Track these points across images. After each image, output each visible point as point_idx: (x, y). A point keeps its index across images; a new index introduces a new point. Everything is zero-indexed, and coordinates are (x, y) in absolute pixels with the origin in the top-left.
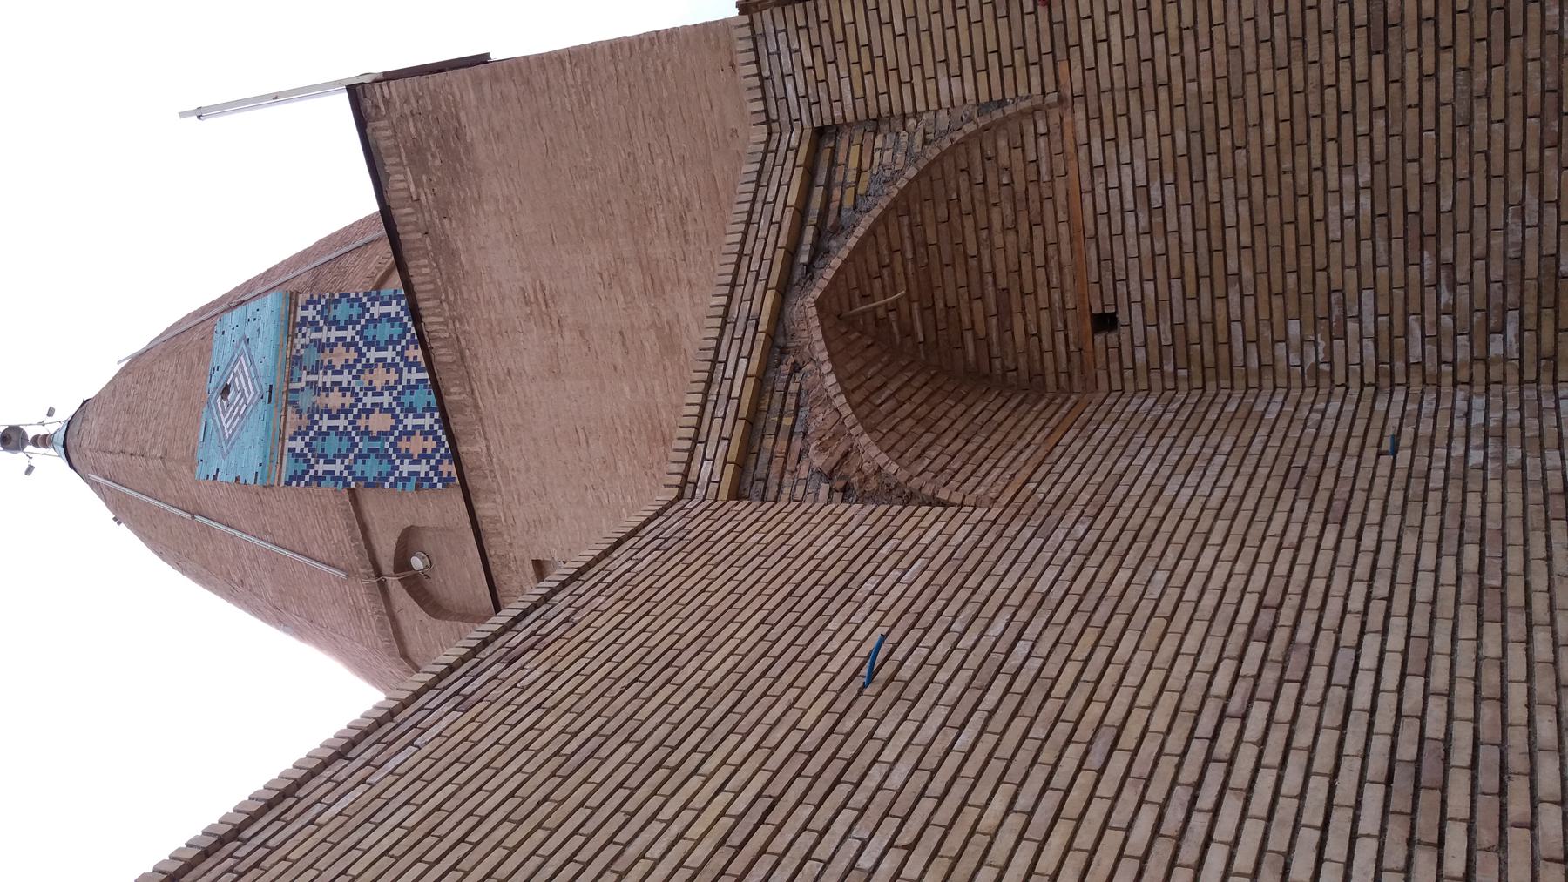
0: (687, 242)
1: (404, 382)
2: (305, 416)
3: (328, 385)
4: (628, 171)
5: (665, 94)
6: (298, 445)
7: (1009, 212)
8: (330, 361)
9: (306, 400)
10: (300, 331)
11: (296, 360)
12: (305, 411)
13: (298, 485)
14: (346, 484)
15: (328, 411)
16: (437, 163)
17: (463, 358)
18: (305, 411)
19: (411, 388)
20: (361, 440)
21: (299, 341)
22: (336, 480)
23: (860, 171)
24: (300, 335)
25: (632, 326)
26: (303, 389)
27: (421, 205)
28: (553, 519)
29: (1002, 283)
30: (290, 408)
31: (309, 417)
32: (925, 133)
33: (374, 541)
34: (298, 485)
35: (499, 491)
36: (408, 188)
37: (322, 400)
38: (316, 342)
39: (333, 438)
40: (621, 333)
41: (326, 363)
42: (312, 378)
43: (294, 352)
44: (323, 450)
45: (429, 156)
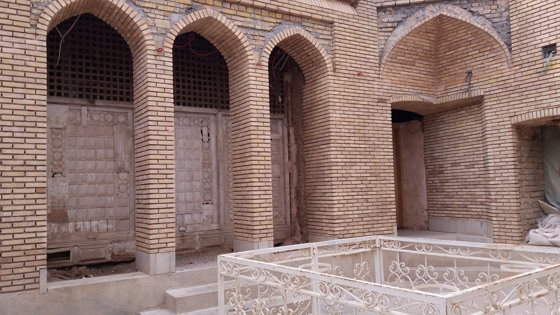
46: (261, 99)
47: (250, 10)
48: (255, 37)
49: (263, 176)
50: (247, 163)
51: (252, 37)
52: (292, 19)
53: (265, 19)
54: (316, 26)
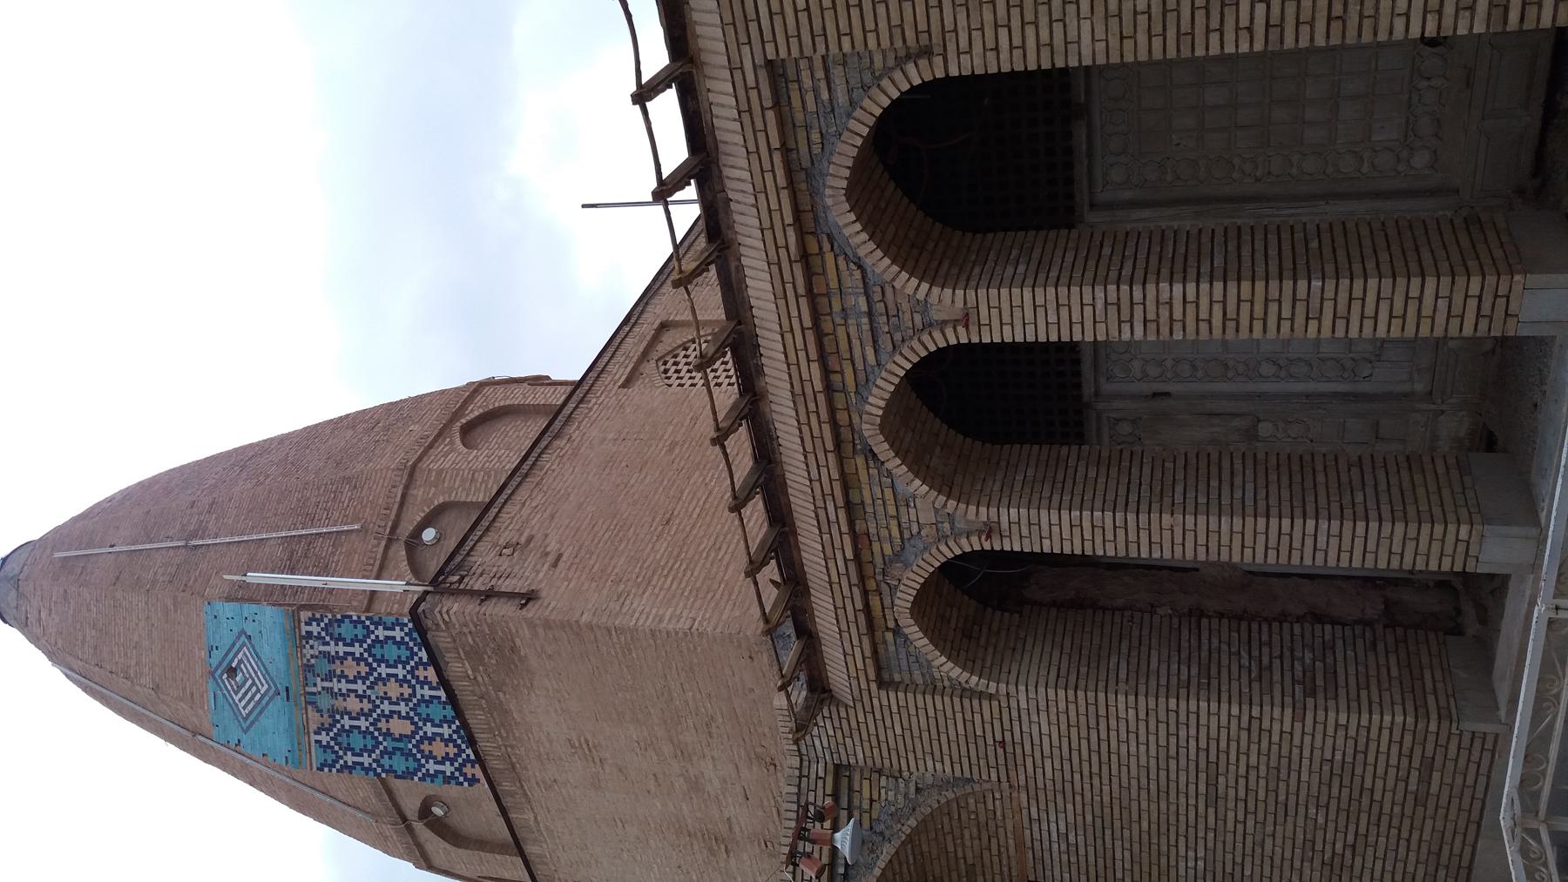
0: (711, 737)
1: (419, 697)
2: (326, 716)
3: (344, 691)
4: (663, 694)
5: (695, 661)
6: (324, 738)
7: (975, 830)
8: (342, 671)
9: (325, 702)
10: (307, 643)
11: (308, 668)
12: (325, 711)
13: (330, 771)
14: (378, 775)
15: (349, 713)
16: (493, 662)
17: (513, 767)
18: (325, 711)
19: (428, 702)
20: (385, 740)
21: (308, 652)
22: (367, 770)
23: (872, 801)
24: (308, 646)
25: (664, 773)
26: (320, 693)
27: (477, 681)
28: (593, 862)
29: (970, 861)
30: (310, 708)
31: (330, 717)
32: (916, 783)
33: (399, 799)
34: (330, 771)
35: (546, 841)
36: (466, 671)
37: (339, 703)
38: (326, 655)
39: (355, 735)
40: (655, 775)
41: (338, 672)
42: (326, 684)
43: (305, 661)
44: (349, 744)
45: (486, 657)
46: (1064, 312)
47: (827, 326)
48: (893, 312)
49: (1301, 308)
50: (1273, 477)
51: (893, 320)
52: (805, 204)
53: (834, 284)
54: (799, 116)
